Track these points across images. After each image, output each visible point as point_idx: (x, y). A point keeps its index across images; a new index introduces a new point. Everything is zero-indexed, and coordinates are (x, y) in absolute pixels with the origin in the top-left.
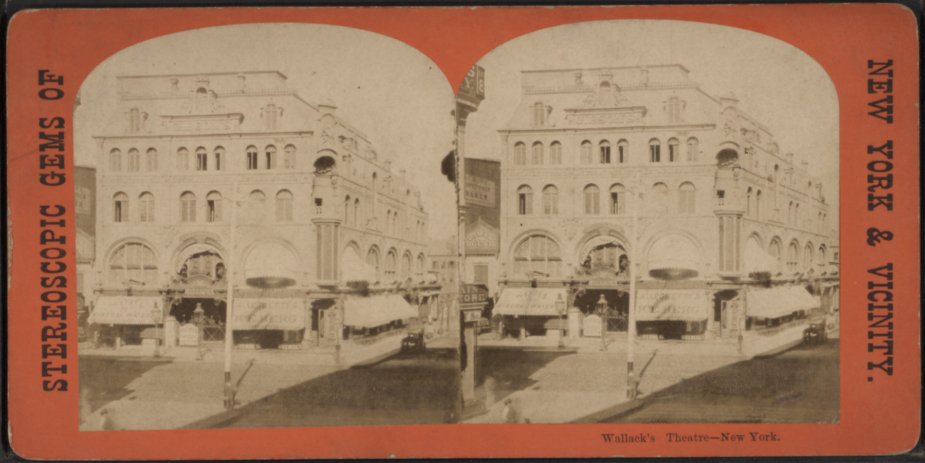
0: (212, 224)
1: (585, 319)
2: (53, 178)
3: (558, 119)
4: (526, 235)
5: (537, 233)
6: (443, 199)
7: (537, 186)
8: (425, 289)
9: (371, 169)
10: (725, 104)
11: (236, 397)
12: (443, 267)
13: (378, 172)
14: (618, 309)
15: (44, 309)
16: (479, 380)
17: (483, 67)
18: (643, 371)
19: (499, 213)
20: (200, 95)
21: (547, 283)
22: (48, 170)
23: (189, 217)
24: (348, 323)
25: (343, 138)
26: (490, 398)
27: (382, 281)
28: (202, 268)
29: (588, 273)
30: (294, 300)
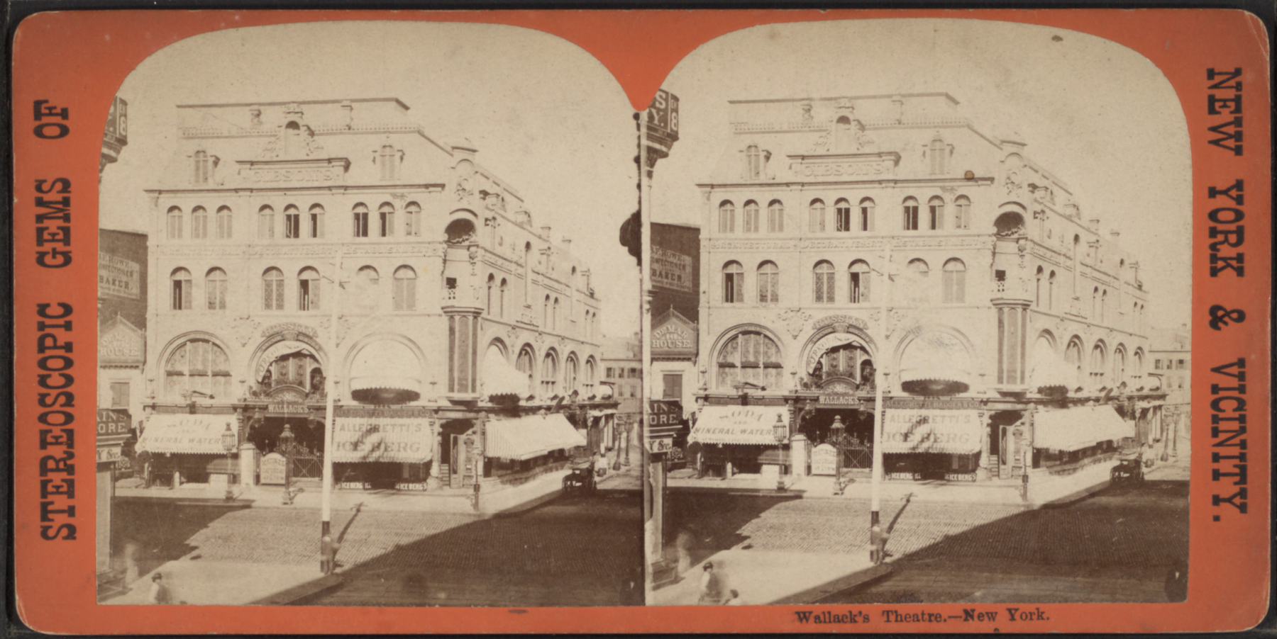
0: (306, 312)
1: (814, 450)
2: (54, 257)
3: (227, 175)
5: (198, 336)
6: (625, 284)
7: (749, 263)
9: (524, 237)
10: (1010, 148)
13: (534, 241)
15: (44, 434)
16: (669, 538)
17: (678, 95)
18: (343, 533)
19: (146, 307)
20: (291, 131)
21: (211, 407)
23: (274, 303)
24: (1040, 444)
25: (485, 194)
26: (683, 562)
27: (537, 395)
28: (291, 375)
29: (819, 386)
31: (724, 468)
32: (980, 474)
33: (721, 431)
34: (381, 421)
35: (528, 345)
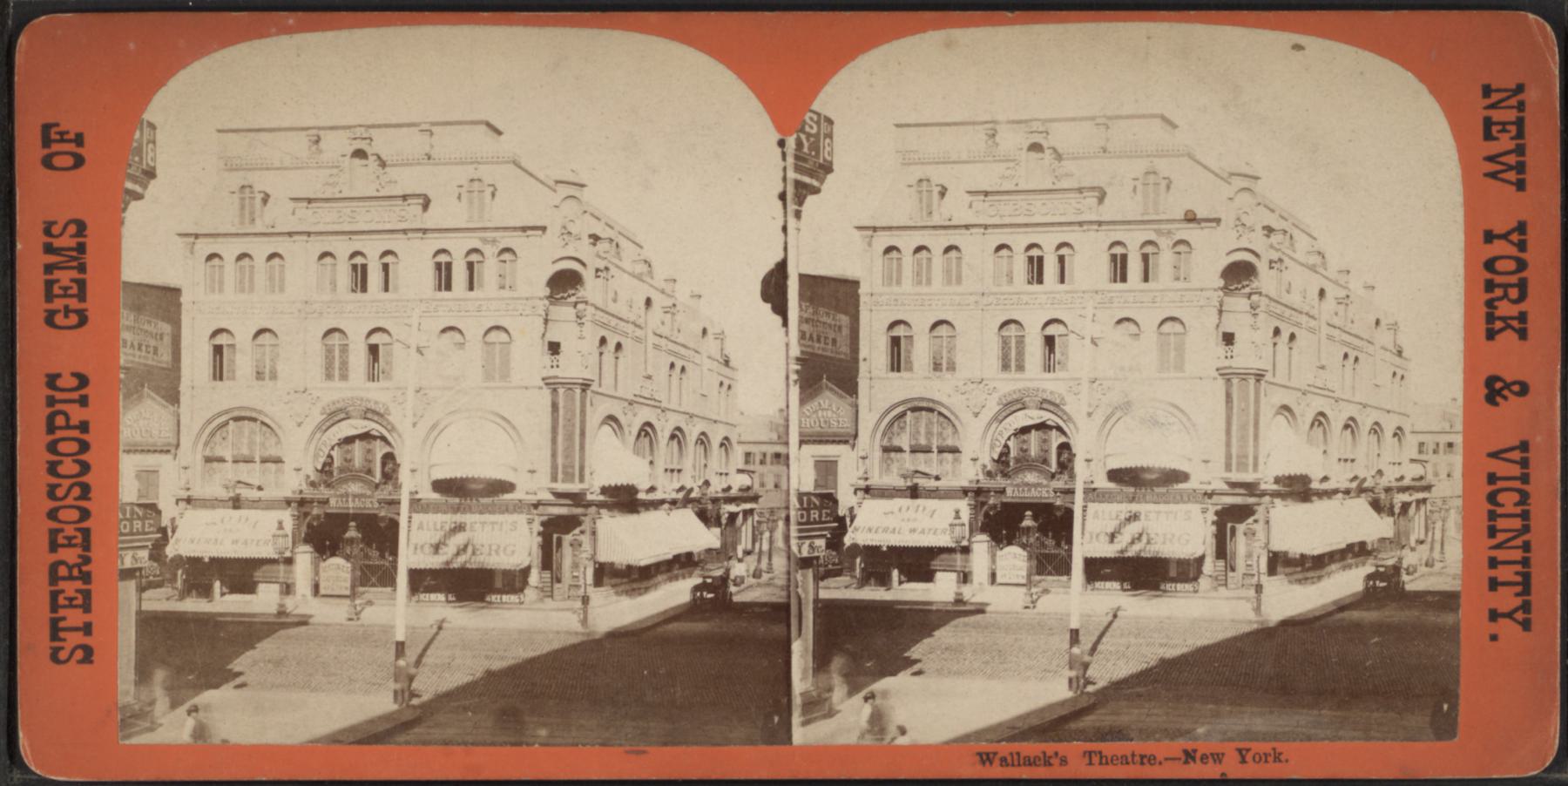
0: (1051, 375)
1: (999, 553)
2: (66, 316)
3: (279, 215)
4: (900, 409)
5: (243, 414)
6: (767, 349)
7: (920, 323)
8: (730, 500)
9: (1316, 283)
10: (564, 191)
11: (414, 685)
12: (1435, 452)
13: (655, 297)
14: (378, 549)
15: (54, 533)
16: (821, 662)
18: (421, 656)
19: (179, 378)
20: (357, 161)
21: (260, 500)
22: (58, 304)
23: (337, 373)
24: (1277, 546)
25: (595, 238)
26: (839, 692)
27: (659, 486)
28: (358, 462)
29: (1005, 475)
30: (514, 517)
31: (889, 576)
32: (1204, 582)
33: (885, 530)
34: (468, 518)
35: (649, 424)
